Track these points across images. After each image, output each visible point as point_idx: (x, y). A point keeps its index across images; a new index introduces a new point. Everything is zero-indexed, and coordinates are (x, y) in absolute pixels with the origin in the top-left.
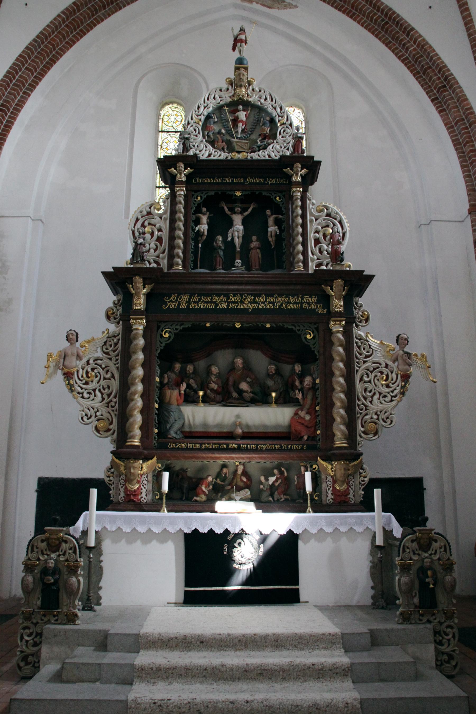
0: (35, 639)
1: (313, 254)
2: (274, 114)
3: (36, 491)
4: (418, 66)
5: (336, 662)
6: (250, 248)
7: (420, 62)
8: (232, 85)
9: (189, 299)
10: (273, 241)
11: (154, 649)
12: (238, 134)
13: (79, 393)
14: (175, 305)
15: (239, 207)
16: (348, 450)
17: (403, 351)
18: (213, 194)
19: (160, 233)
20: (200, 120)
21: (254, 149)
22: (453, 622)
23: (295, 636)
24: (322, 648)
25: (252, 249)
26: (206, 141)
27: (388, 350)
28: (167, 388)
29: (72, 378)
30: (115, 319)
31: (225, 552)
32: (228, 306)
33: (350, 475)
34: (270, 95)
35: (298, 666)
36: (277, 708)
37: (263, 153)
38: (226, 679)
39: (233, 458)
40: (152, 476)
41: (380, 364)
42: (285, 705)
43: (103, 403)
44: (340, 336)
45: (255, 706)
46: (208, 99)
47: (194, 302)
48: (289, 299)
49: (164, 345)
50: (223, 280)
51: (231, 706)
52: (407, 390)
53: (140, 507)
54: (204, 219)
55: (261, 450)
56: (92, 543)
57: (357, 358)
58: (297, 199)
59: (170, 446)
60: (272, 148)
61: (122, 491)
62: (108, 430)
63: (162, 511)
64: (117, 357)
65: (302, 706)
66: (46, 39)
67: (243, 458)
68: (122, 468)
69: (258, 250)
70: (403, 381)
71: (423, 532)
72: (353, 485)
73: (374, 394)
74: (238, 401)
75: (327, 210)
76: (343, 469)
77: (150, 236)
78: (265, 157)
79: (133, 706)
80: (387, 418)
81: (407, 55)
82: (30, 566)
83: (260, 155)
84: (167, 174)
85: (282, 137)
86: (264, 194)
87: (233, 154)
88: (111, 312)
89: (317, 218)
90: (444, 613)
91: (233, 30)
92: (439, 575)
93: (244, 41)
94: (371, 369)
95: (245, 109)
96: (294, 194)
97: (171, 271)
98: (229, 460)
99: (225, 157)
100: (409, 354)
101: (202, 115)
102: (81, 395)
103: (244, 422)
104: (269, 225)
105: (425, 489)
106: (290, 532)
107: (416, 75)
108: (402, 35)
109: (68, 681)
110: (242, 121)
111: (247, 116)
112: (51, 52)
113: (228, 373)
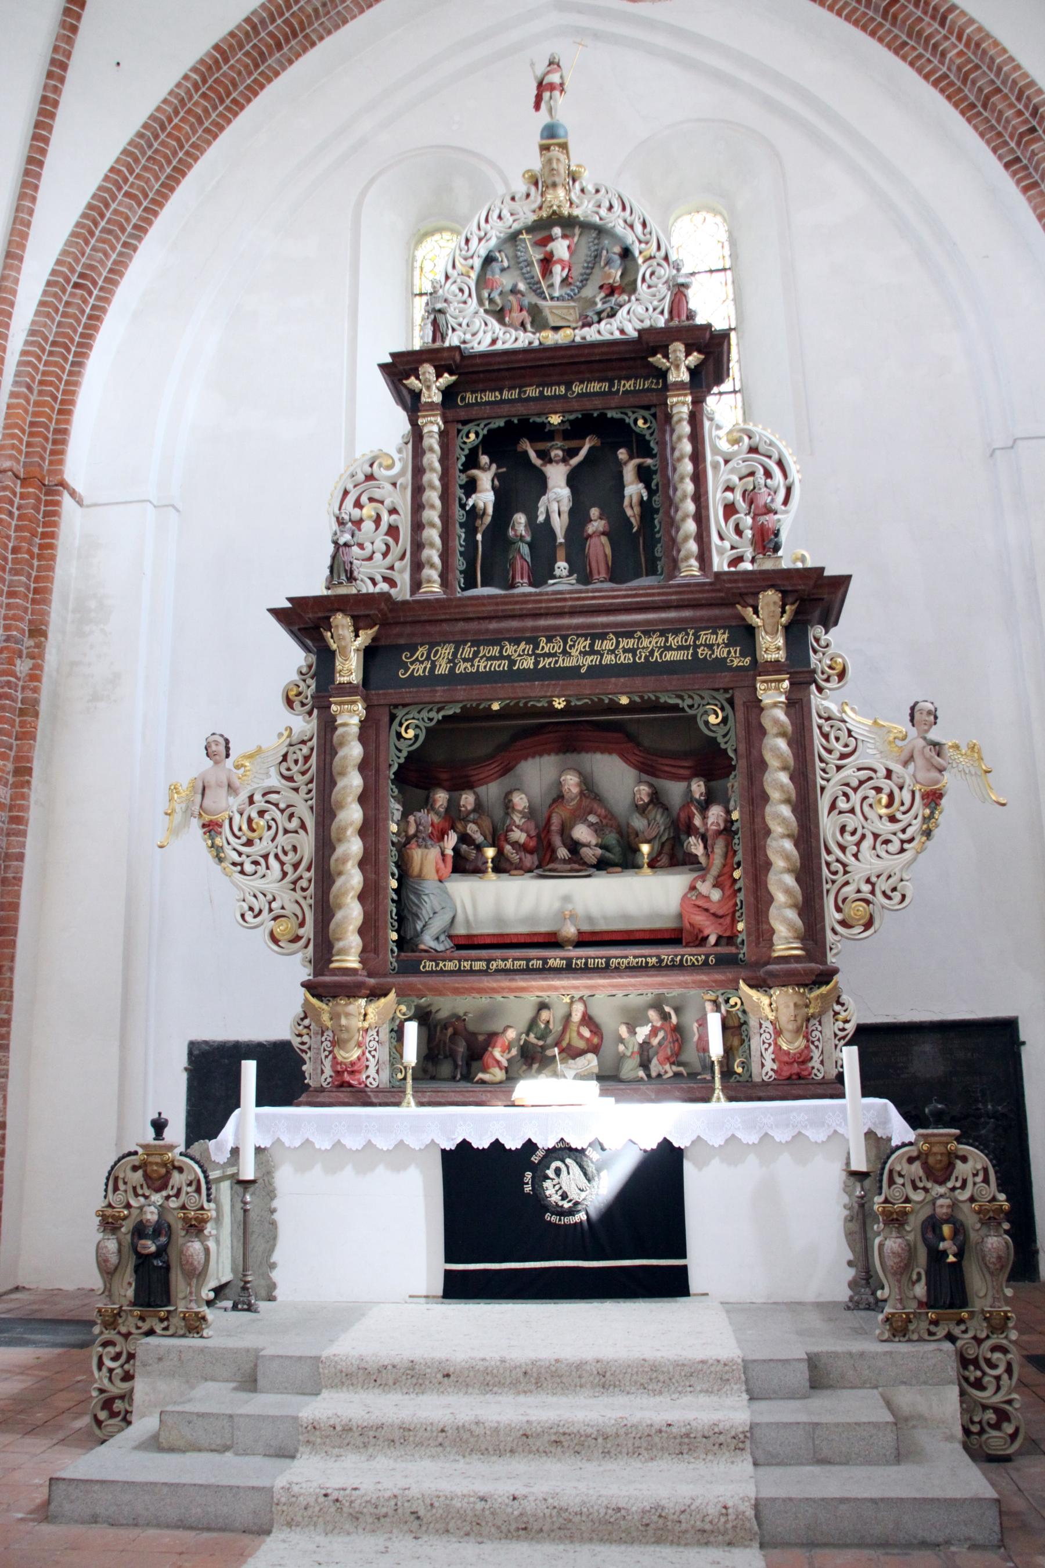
0: (126, 1367)
1: (721, 538)
2: (630, 238)
3: (186, 1069)
4: (970, 91)
5: (720, 1421)
6: (585, 535)
7: (974, 83)
8: (536, 184)
9: (455, 655)
10: (634, 516)
11: (351, 1388)
12: (554, 290)
13: (234, 864)
14: (425, 668)
15: (557, 448)
16: (800, 963)
17: (925, 739)
18: (502, 424)
19: (394, 517)
20: (472, 268)
21: (589, 319)
22: (1006, 1337)
23: (642, 1366)
24: (701, 1391)
25: (590, 536)
26: (486, 311)
27: (891, 739)
28: (414, 846)
29: (220, 833)
30: (303, 705)
31: (528, 1189)
32: (537, 663)
33: (813, 1016)
34: (620, 198)
35: (637, 1428)
36: (576, 1514)
37: (608, 326)
38: (485, 1452)
39: (556, 988)
40: (388, 1030)
41: (875, 771)
42: (592, 1507)
43: (285, 881)
44: (780, 715)
45: (528, 1508)
46: (487, 221)
47: (465, 660)
48: (667, 640)
49: (404, 754)
50: (521, 609)
51: (480, 1505)
52: (937, 826)
53: (362, 1097)
54: (485, 479)
55: (617, 969)
56: (248, 1173)
57: (822, 760)
58: (680, 420)
59: (424, 967)
60: (628, 312)
61: (328, 1063)
62: (297, 939)
63: (404, 1104)
64: (310, 786)
65: (627, 1510)
66: (163, 128)
67: (576, 988)
68: (325, 1018)
69: (604, 539)
70: (926, 805)
71: (933, 1139)
72: (819, 1040)
73: (863, 837)
74: (568, 867)
75: (750, 438)
76: (792, 1005)
77: (373, 526)
78: (612, 334)
79: (283, 1500)
80: (894, 889)
81: (945, 69)
82: (110, 1220)
83: (602, 331)
84: (405, 392)
85: (649, 287)
86: (609, 415)
87: (544, 334)
88: (294, 692)
89: (728, 458)
90: (986, 1319)
91: (532, 64)
92: (973, 1236)
93: (558, 87)
94: (855, 783)
95: (568, 233)
96: (675, 411)
97: (417, 597)
98: (548, 993)
99: (527, 343)
100: (937, 746)
101: (475, 258)
102: (239, 868)
103: (580, 910)
104: (626, 482)
105: (1024, 1043)
106: (666, 1144)
107: (967, 110)
108: (929, 25)
109: (171, 1450)
110: (560, 261)
111: (573, 246)
112: (175, 154)
113: (550, 806)
